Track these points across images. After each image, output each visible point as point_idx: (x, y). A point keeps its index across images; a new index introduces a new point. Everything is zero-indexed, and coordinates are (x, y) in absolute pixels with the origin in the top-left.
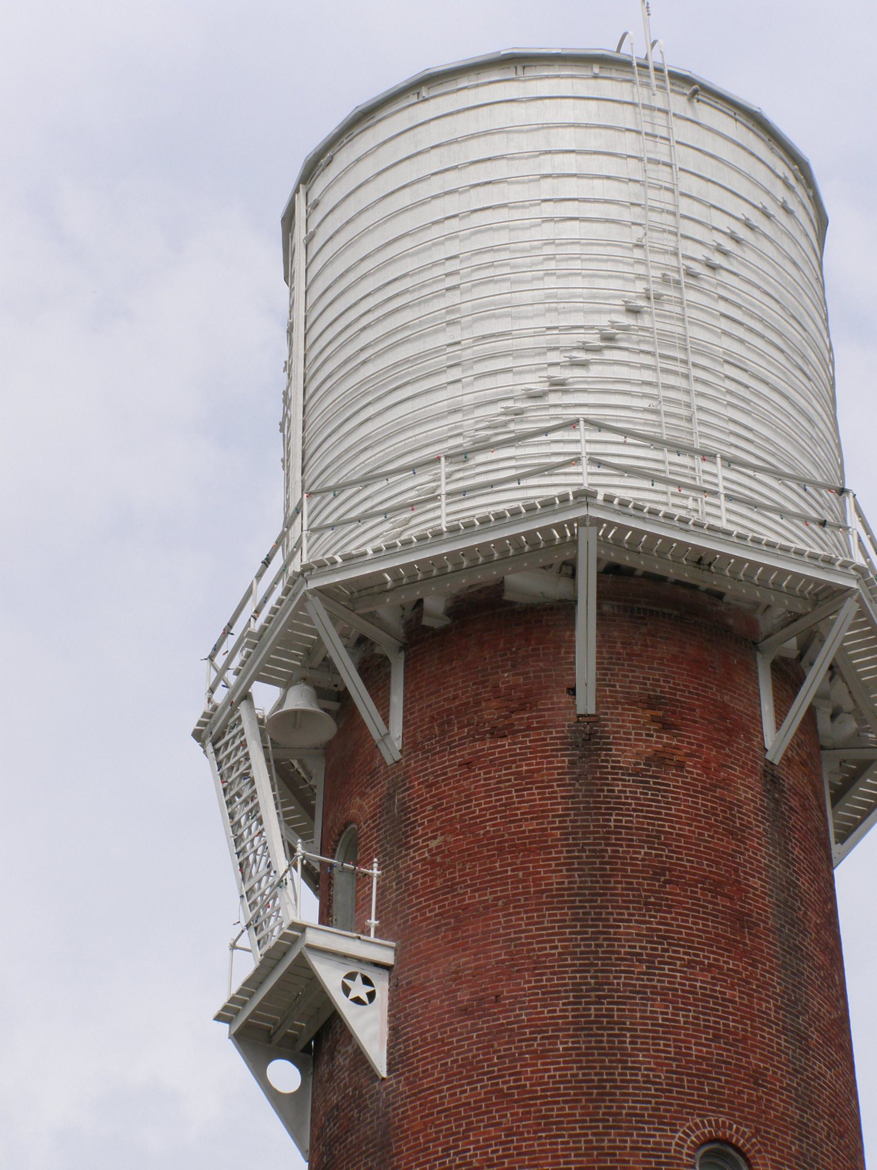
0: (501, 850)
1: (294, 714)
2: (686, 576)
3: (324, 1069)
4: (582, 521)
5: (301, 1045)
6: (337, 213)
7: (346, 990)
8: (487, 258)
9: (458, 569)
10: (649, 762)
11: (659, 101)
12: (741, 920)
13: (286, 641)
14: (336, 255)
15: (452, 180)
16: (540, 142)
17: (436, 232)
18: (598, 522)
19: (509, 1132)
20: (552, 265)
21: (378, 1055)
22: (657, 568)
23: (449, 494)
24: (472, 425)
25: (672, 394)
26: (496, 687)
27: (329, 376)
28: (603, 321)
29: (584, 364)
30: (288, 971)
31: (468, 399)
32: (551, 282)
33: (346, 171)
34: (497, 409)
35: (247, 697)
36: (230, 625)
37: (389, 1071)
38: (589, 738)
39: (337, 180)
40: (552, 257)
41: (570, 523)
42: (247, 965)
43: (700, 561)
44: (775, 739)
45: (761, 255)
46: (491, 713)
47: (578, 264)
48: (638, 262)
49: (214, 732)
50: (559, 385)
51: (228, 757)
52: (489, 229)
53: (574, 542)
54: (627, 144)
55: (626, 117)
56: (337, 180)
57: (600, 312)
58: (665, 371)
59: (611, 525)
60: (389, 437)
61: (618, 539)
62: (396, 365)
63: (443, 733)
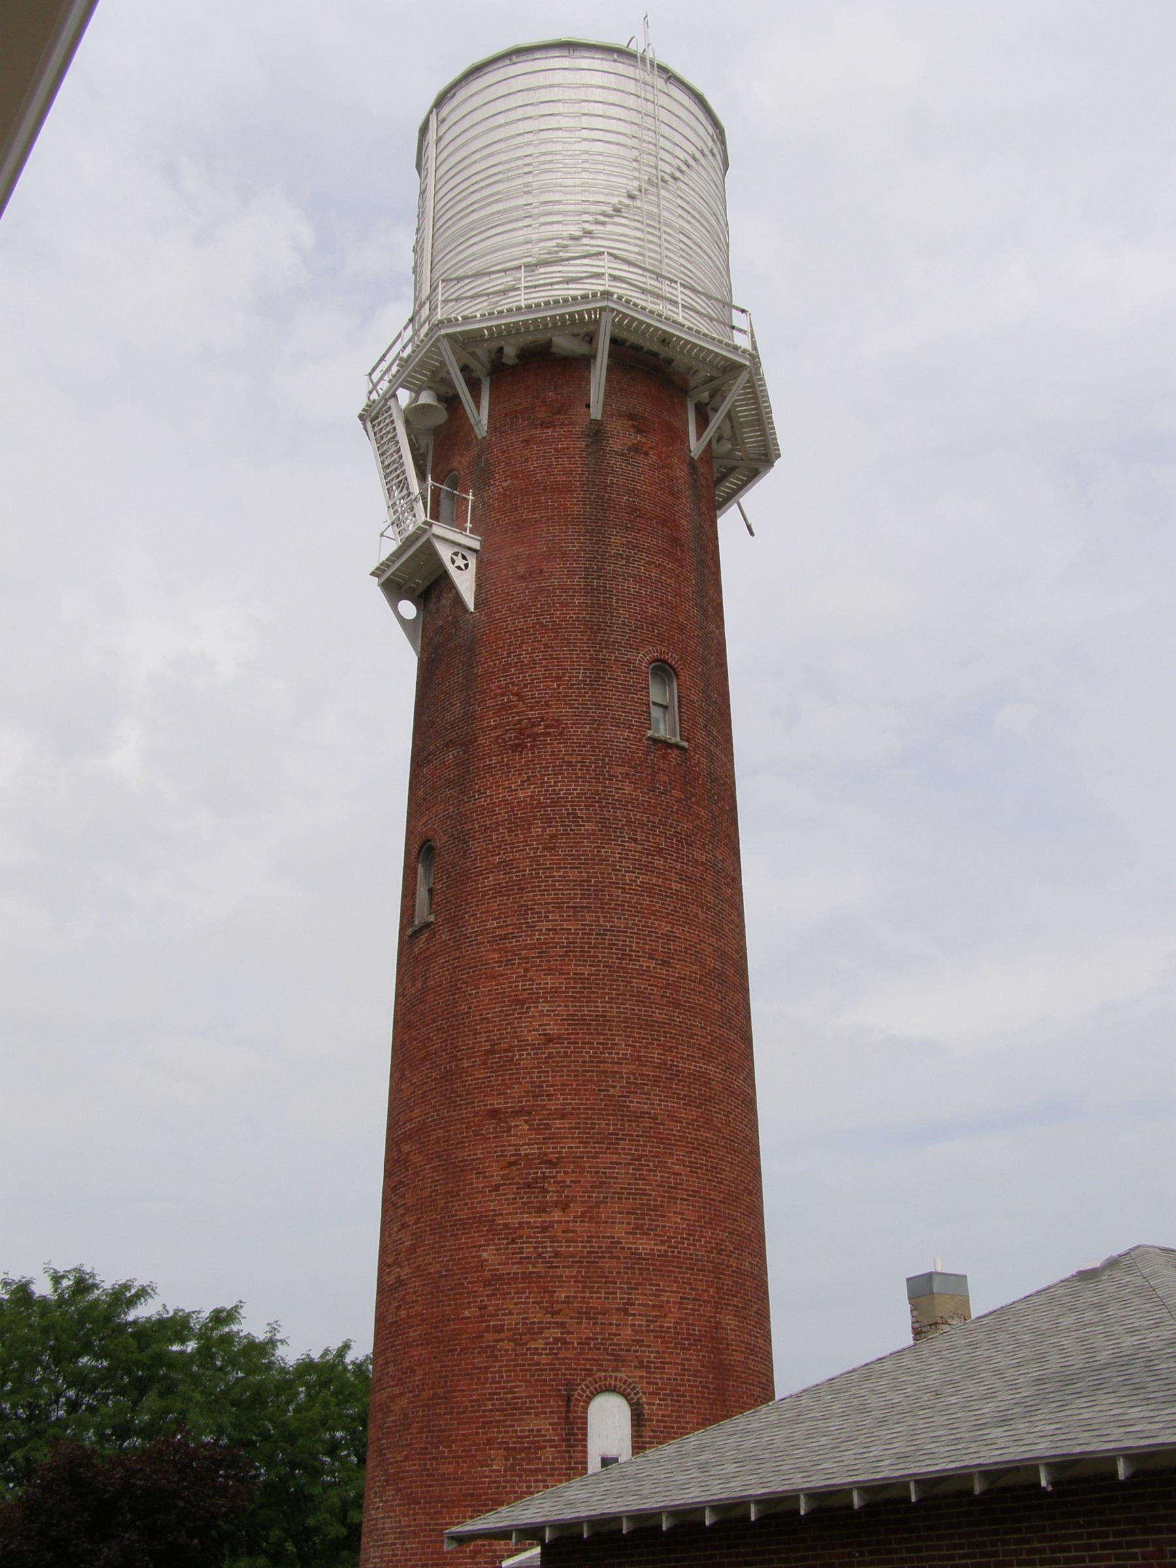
0: (545, 490)
1: (424, 406)
2: (656, 348)
3: (432, 607)
4: (602, 309)
5: (417, 593)
6: (457, 126)
7: (453, 562)
8: (549, 158)
9: (527, 331)
10: (629, 449)
11: (649, 79)
12: (676, 542)
13: (422, 364)
14: (456, 150)
15: (529, 111)
16: (582, 94)
17: (519, 140)
18: (613, 310)
19: (546, 646)
20: (587, 165)
21: (469, 599)
22: (640, 342)
23: (526, 288)
24: (537, 252)
25: (652, 246)
26: (544, 400)
27: (450, 219)
28: (615, 200)
29: (603, 223)
30: (418, 550)
31: (535, 237)
32: (585, 175)
33: (464, 101)
34: (554, 243)
35: (394, 396)
36: (384, 356)
37: (475, 608)
38: (597, 433)
39: (458, 106)
40: (587, 161)
41: (595, 309)
42: (391, 546)
43: (664, 341)
44: (695, 446)
45: (700, 175)
46: (541, 414)
47: (601, 167)
48: (635, 169)
49: (373, 416)
50: (588, 234)
51: (381, 430)
52: (551, 141)
53: (597, 322)
54: (631, 102)
55: (631, 86)
56: (458, 106)
57: (613, 195)
58: (649, 233)
59: (619, 312)
60: (493, 252)
61: (620, 322)
62: (493, 214)
63: (512, 423)
